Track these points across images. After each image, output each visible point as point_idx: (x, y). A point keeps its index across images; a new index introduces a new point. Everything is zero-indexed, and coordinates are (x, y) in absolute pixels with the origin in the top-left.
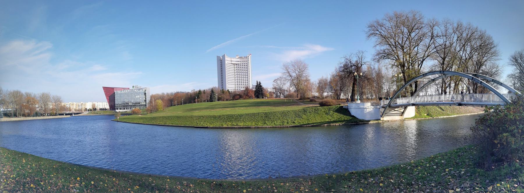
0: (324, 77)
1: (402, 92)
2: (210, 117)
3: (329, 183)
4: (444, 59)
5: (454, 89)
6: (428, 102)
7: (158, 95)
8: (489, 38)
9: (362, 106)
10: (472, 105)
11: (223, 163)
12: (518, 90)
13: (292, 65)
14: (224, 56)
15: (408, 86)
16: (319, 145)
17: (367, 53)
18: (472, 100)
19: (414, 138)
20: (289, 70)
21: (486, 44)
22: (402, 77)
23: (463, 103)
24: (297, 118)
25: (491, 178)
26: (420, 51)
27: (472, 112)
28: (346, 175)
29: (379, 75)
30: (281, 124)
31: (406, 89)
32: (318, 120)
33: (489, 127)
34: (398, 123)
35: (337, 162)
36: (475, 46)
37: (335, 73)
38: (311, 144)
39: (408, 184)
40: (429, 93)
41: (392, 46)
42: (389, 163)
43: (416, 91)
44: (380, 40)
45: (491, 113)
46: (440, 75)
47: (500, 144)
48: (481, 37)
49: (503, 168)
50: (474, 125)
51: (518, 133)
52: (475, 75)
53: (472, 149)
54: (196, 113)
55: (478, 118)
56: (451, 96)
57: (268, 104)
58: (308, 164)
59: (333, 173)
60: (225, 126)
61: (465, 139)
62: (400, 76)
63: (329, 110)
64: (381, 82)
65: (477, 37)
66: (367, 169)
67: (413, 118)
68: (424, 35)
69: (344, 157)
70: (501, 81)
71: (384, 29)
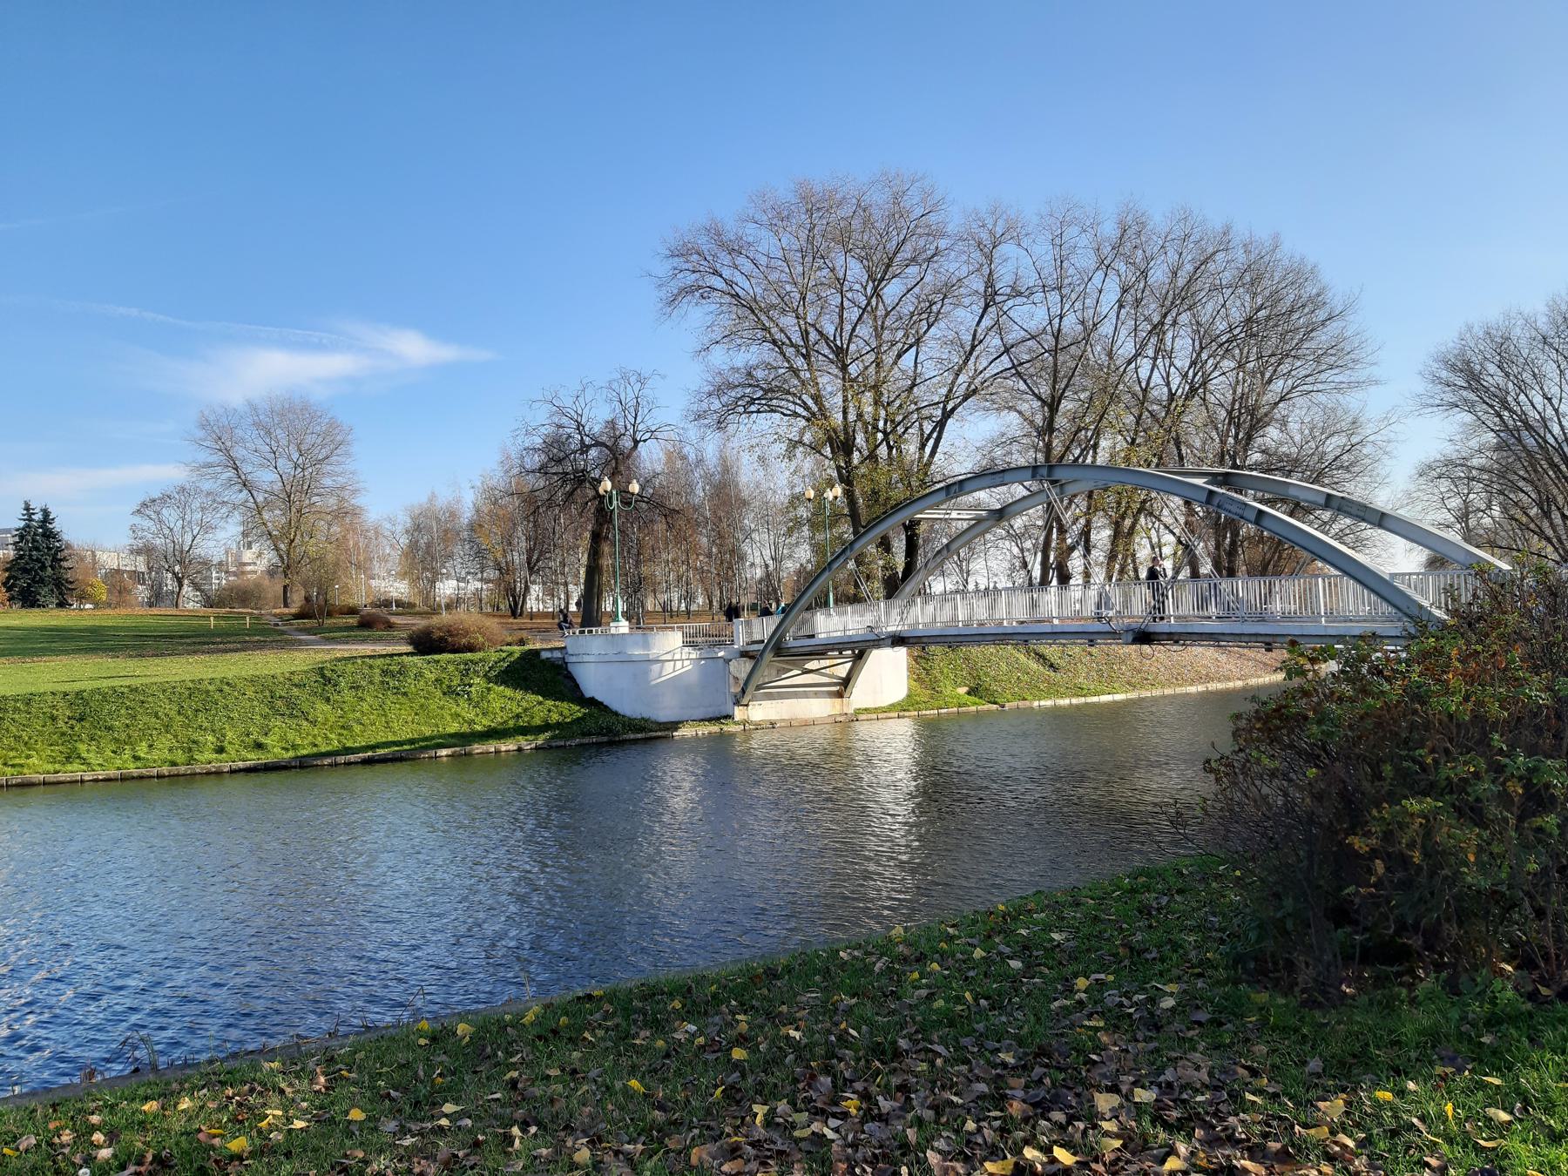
0: (444, 498)
1: (841, 576)
3: (431, 1067)
4: (1052, 405)
5: (1112, 557)
6: (990, 628)
8: (1298, 275)
9: (637, 652)
10: (1213, 638)
12: (1492, 545)
15: (872, 549)
17: (667, 386)
18: (1213, 610)
19: (903, 811)
20: (238, 452)
21: (1283, 307)
22: (842, 503)
23: (1160, 627)
24: (277, 722)
25: (1336, 1048)
26: (928, 369)
27: (1209, 678)
29: (726, 495)
30: (180, 756)
31: (859, 563)
32: (404, 726)
33: (1312, 759)
34: (822, 736)
36: (1221, 326)
37: (498, 479)
39: (877, 1051)
40: (979, 579)
41: (790, 351)
42: (776, 940)
43: (909, 569)
44: (727, 321)
45: (1322, 682)
46: (1035, 486)
47: (1388, 858)
48: (1251, 276)
49: (1413, 1001)
50: (1226, 745)
51: (1505, 798)
52: (1225, 480)
53: (1218, 877)
55: (1249, 708)
56: (1093, 593)
57: (95, 641)
61: (1178, 820)
62: (829, 495)
63: (465, 673)
64: (735, 525)
65: (1227, 277)
66: (666, 975)
67: (900, 709)
68: (947, 290)
70: (1382, 500)
71: (747, 266)
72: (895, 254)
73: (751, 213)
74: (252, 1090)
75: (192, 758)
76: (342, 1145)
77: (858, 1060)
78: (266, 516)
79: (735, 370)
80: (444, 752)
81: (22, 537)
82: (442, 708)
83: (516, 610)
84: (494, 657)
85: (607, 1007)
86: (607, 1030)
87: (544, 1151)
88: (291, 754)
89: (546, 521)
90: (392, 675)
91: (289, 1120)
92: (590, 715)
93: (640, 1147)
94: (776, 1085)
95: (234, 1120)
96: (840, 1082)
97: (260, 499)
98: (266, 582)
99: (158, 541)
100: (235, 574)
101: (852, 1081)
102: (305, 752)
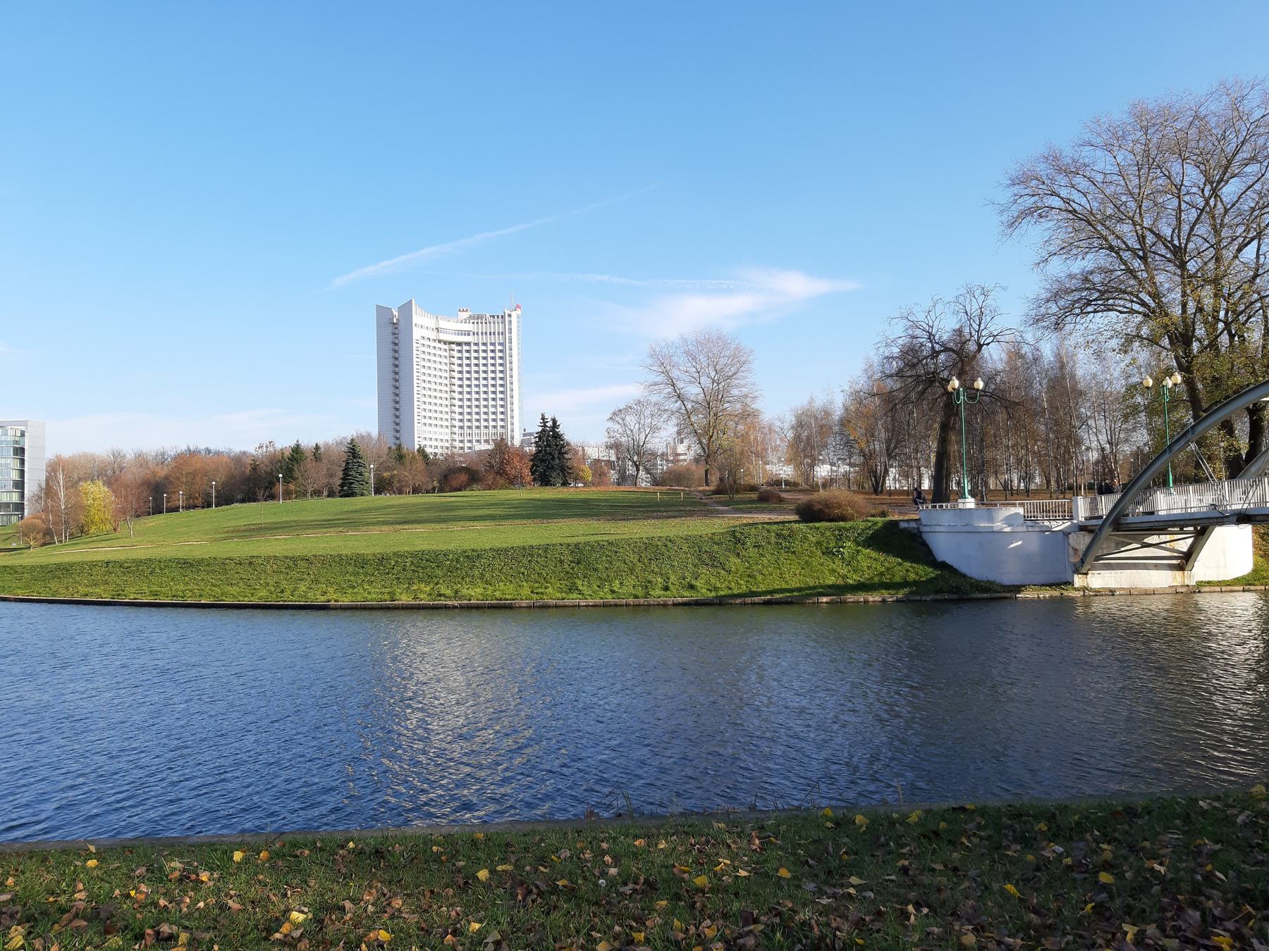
0: (820, 402)
1: (1181, 456)
2: (340, 560)
3: (838, 846)
7: (91, 459)
11: (391, 757)
13: (688, 353)
14: (406, 309)
16: (796, 684)
20: (675, 373)
24: (703, 570)
28: (913, 818)
29: (1062, 386)
30: (640, 592)
31: (1199, 444)
32: (792, 577)
34: (1159, 605)
35: (874, 758)
37: (862, 383)
38: (761, 678)
41: (1126, 255)
54: (279, 546)
57: (585, 509)
58: (750, 762)
59: (853, 807)
60: (405, 599)
62: (1169, 383)
63: (839, 538)
67: (1245, 583)
69: (904, 742)
72: (1234, 156)
73: (1085, 137)
74: (707, 842)
75: (648, 593)
76: (775, 895)
77: (1227, 901)
78: (693, 419)
79: (1071, 276)
80: (825, 599)
81: (540, 438)
82: (822, 565)
83: (878, 488)
84: (862, 525)
85: (978, 819)
86: (981, 838)
87: (936, 930)
88: (713, 594)
89: (902, 416)
90: (784, 538)
91: (736, 869)
92: (941, 576)
93: (1019, 941)
94: (1144, 911)
95: (697, 862)
96: (1210, 919)
97: (689, 407)
98: (694, 467)
99: (623, 439)
100: (672, 462)
101: (1222, 920)
102: (722, 593)
